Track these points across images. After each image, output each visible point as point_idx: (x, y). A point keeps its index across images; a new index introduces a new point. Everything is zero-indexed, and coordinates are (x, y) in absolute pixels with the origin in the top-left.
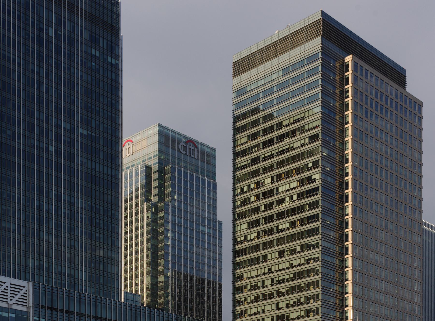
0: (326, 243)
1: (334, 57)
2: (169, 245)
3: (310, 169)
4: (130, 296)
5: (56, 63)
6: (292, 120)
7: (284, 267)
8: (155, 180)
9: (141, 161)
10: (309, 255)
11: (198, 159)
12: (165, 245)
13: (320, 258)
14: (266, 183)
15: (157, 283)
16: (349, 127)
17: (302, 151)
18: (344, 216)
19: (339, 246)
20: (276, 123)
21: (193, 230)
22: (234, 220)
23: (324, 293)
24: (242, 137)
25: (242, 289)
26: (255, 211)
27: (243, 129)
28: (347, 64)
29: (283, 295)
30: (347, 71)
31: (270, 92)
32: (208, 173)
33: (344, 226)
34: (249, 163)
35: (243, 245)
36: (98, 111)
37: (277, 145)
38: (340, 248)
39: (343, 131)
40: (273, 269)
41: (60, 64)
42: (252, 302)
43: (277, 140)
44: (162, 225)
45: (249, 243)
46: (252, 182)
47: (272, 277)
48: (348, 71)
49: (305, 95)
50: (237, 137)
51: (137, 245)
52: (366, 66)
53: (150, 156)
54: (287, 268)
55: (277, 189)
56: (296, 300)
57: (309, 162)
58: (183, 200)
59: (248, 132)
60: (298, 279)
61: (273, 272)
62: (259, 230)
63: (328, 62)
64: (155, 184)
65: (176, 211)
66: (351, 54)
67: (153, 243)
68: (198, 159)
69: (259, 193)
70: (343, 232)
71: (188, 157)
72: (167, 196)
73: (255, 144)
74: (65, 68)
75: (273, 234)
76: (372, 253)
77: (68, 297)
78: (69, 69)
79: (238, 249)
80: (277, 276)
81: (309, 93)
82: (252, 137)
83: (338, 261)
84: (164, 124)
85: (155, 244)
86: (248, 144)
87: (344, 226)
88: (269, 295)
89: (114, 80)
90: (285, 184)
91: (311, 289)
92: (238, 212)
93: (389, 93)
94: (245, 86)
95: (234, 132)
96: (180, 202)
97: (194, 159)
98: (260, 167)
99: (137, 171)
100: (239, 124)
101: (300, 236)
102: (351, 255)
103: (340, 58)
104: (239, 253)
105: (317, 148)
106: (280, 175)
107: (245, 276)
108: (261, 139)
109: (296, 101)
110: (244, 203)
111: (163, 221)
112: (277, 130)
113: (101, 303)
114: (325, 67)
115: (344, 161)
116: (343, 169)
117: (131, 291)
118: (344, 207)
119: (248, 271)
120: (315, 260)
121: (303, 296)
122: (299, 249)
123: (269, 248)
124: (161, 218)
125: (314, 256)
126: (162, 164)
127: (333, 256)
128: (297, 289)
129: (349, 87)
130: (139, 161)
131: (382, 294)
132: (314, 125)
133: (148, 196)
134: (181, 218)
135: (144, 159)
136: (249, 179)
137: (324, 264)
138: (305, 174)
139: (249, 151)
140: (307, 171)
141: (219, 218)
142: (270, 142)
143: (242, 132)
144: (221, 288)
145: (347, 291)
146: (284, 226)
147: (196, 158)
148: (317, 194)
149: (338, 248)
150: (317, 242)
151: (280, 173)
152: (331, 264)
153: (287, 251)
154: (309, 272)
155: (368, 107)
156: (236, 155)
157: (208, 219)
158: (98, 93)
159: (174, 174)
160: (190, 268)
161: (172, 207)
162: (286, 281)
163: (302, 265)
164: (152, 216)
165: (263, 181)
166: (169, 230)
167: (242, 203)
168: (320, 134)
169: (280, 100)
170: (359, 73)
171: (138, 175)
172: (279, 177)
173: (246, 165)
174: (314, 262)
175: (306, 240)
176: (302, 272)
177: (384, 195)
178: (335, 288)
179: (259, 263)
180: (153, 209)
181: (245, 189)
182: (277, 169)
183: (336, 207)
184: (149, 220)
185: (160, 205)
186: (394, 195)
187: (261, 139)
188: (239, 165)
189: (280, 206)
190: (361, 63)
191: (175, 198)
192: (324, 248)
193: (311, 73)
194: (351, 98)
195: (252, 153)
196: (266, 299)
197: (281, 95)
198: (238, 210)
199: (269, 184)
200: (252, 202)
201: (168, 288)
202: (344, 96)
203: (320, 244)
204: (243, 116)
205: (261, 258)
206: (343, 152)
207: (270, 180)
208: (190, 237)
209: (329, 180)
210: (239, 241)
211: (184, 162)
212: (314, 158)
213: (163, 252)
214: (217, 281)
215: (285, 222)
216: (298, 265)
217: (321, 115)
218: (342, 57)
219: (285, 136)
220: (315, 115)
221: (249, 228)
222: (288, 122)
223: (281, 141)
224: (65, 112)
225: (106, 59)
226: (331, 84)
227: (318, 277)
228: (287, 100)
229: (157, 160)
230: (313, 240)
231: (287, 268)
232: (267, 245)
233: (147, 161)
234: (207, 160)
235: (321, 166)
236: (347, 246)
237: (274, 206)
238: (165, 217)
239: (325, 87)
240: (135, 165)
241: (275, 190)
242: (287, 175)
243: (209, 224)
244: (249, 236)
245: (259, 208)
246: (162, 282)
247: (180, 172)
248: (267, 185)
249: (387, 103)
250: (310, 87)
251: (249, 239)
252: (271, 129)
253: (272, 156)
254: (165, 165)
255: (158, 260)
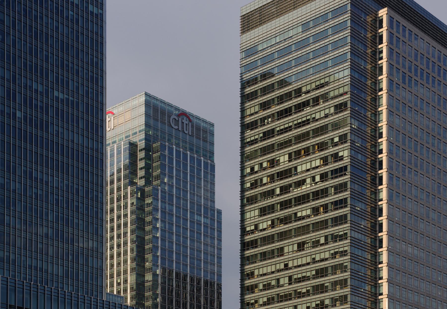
0: (356, 233)
1: (365, 10)
2: (158, 238)
3: (336, 145)
4: (111, 297)
5: (25, 10)
6: (313, 86)
7: (304, 262)
8: (141, 159)
9: (124, 136)
10: (335, 248)
11: (192, 136)
12: (154, 236)
13: (349, 251)
14: (282, 160)
15: (144, 282)
16: (384, 94)
17: (326, 123)
18: (378, 201)
19: (371, 238)
20: (294, 89)
21: (187, 220)
22: (243, 206)
23: (354, 294)
24: (253, 106)
25: (252, 289)
26: (269, 195)
27: (253, 96)
28: (381, 18)
29: (303, 297)
30: (381, 27)
31: (286, 51)
32: (205, 153)
33: (377, 214)
34: (261, 137)
35: (253, 236)
36: (78, 71)
37: (296, 116)
38: (373, 240)
39: (376, 99)
40: (290, 265)
41: (31, 12)
42: (264, 304)
43: (295, 109)
44: (150, 213)
45: (261, 233)
46: (264, 160)
47: (290, 275)
48: (382, 27)
49: (331, 55)
50: (246, 105)
51: (119, 236)
52: (404, 22)
53: (135, 131)
54: (308, 264)
55: (296, 168)
56: (319, 302)
57: (335, 136)
58: (174, 184)
59: (260, 99)
60: (322, 277)
61: (291, 269)
62: (273, 218)
63: (358, 15)
64: (141, 164)
65: (167, 198)
66: (386, 7)
67: (139, 235)
68: (192, 136)
69: (272, 173)
70: (376, 221)
71: (181, 133)
72: (155, 178)
73: (268, 114)
74: (36, 17)
75: (290, 222)
76: (411, 246)
77: (43, 295)
78: (42, 18)
79: (247, 240)
80: (296, 273)
81: (335, 53)
82: (264, 106)
83: (370, 255)
84: (152, 93)
85: (141, 236)
86: (260, 114)
87: (377, 214)
88: (286, 296)
89: (97, 34)
90: (305, 162)
91: (338, 289)
92: (248, 196)
93: (431, 55)
94: (256, 44)
95: (242, 100)
96: (171, 186)
97: (188, 136)
98: (274, 142)
99: (119, 148)
100: (248, 90)
101: (323, 224)
102: (386, 249)
103: (372, 12)
104: (248, 246)
105: (344, 119)
106: (299, 151)
107: (256, 273)
108: (275, 109)
109: (319, 63)
110: (254, 185)
111: (151, 208)
112: (296, 97)
113: (85, 303)
114: (355, 22)
115: (377, 136)
116: (376, 145)
117: (113, 291)
118: (377, 191)
119: (260, 267)
120: (343, 254)
121: (328, 297)
122: (322, 241)
123: (286, 239)
124: (149, 205)
125: (341, 250)
126: (150, 141)
127: (364, 249)
128: (320, 289)
129: (384, 47)
130: (121, 137)
131: (423, 296)
132: (341, 91)
133: (133, 179)
134: (173, 205)
135: (128, 134)
136: (261, 156)
137: (354, 259)
138: (330, 150)
139: (261, 123)
140: (333, 146)
141: (218, 206)
142: (287, 112)
143: (252, 100)
144: (221, 288)
145: (381, 292)
146: (304, 213)
147: (190, 134)
148: (345, 174)
149: (370, 240)
150: (345, 232)
151: (299, 149)
152: (363, 259)
153: (308, 243)
154: (335, 268)
155: (406, 71)
156: (245, 127)
157: (204, 207)
158: (78, 49)
159: (164, 152)
160: (183, 264)
161: (162, 191)
162: (307, 279)
163: (326, 259)
164: (137, 202)
165: (278, 159)
166: (158, 219)
167: (252, 184)
168: (349, 103)
169: (299, 61)
170: (395, 30)
171: (121, 153)
172: (298, 154)
173: (257, 139)
174: (341, 256)
175: (331, 230)
176: (326, 268)
177: (425, 177)
178: (367, 289)
179: (273, 257)
180: (139, 194)
181: (256, 168)
182: (295, 144)
183: (367, 191)
184: (134, 208)
185: (147, 189)
186: (436, 177)
187: (275, 109)
188: (248, 140)
189: (299, 189)
190: (397, 17)
191: (165, 181)
192: (354, 239)
193: (337, 29)
194: (386, 60)
195: (264, 125)
196: (281, 301)
197: (300, 55)
198: (248, 194)
199: (285, 163)
200: (265, 184)
201: (157, 288)
202: (378, 57)
203: (349, 235)
204: (254, 81)
205: (276, 251)
206: (376, 125)
207: (287, 157)
208: (183, 228)
209: (360, 158)
210: (249, 231)
211: (176, 138)
212: (341, 131)
213: (150, 246)
214: (216, 280)
215: (305, 208)
216: (322, 260)
217: (349, 79)
218: (375, 11)
219: (305, 104)
220: (338, 81)
221: (260, 216)
222: (309, 88)
223: (300, 111)
224: (36, 71)
225: (87, 8)
226: (361, 42)
227: (347, 275)
228: (308, 61)
229: (143, 136)
230: (340, 230)
231: (308, 264)
232: (283, 236)
233: (131, 137)
234: (203, 137)
235: (349, 141)
236: (380, 238)
237: (291, 189)
238: (154, 203)
239: (355, 45)
240: (117, 141)
241: (293, 169)
242: (307, 151)
243: (206, 213)
244: (261, 225)
245: (273, 191)
246: (150, 281)
247: (171, 150)
248: (283, 164)
249: (428, 67)
250: (336, 45)
251: (261, 228)
252: (288, 96)
253: (289, 129)
254: (153, 142)
255: (145, 254)
